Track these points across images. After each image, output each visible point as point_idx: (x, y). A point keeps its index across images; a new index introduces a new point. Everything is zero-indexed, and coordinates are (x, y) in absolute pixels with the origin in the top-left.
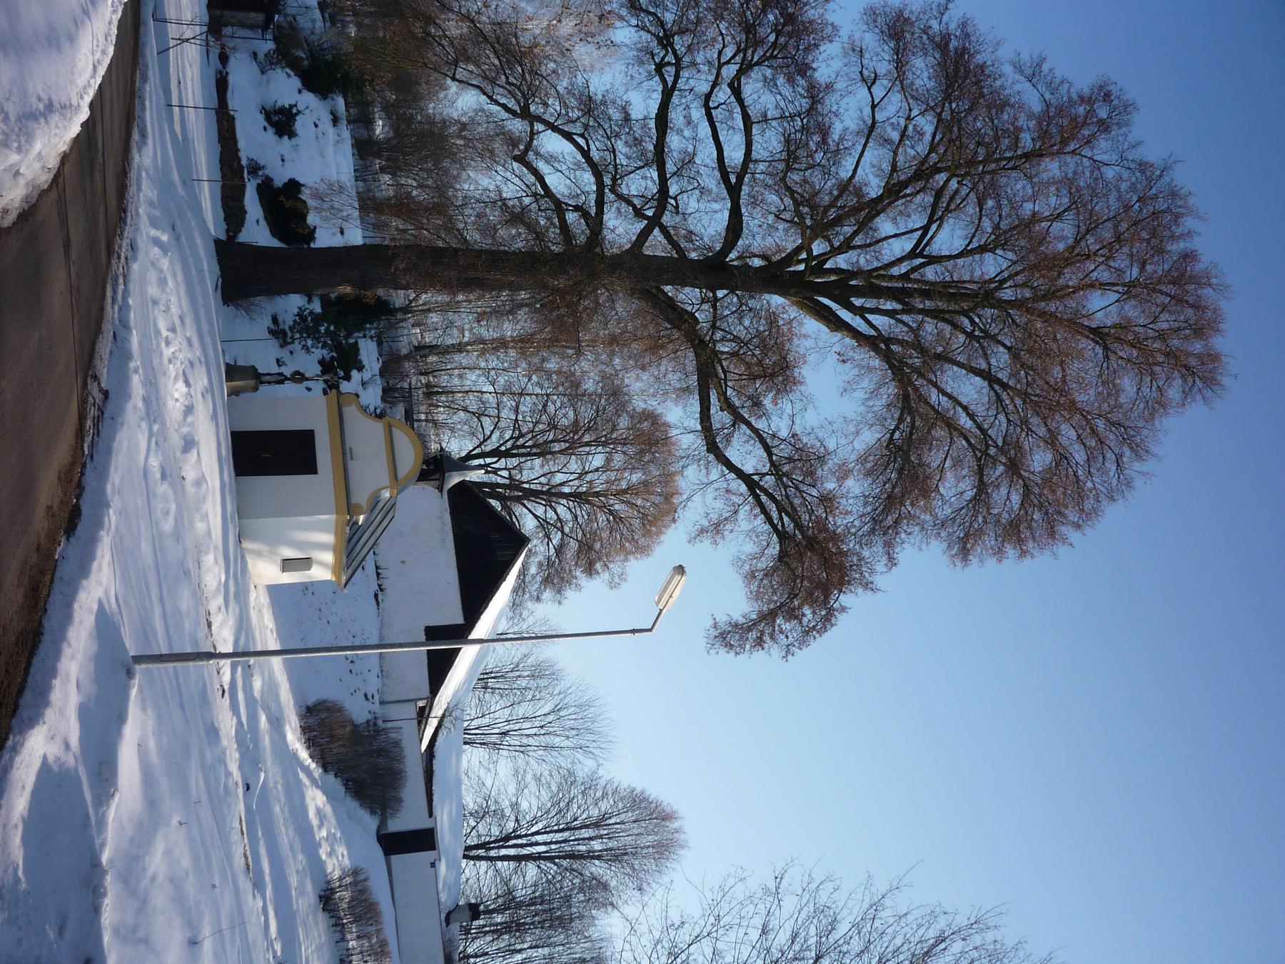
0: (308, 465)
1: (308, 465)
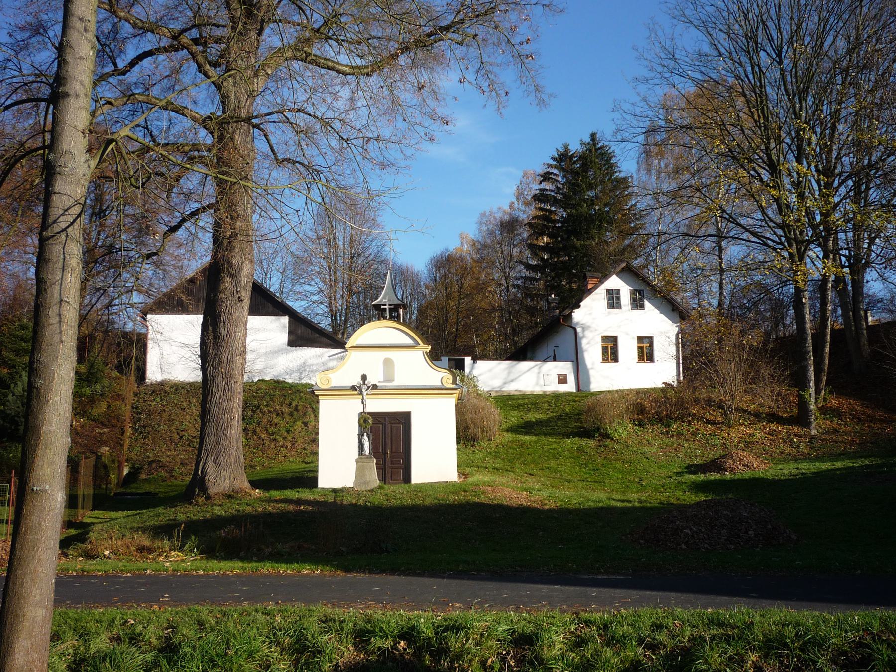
0: (404, 419)
1: (404, 419)
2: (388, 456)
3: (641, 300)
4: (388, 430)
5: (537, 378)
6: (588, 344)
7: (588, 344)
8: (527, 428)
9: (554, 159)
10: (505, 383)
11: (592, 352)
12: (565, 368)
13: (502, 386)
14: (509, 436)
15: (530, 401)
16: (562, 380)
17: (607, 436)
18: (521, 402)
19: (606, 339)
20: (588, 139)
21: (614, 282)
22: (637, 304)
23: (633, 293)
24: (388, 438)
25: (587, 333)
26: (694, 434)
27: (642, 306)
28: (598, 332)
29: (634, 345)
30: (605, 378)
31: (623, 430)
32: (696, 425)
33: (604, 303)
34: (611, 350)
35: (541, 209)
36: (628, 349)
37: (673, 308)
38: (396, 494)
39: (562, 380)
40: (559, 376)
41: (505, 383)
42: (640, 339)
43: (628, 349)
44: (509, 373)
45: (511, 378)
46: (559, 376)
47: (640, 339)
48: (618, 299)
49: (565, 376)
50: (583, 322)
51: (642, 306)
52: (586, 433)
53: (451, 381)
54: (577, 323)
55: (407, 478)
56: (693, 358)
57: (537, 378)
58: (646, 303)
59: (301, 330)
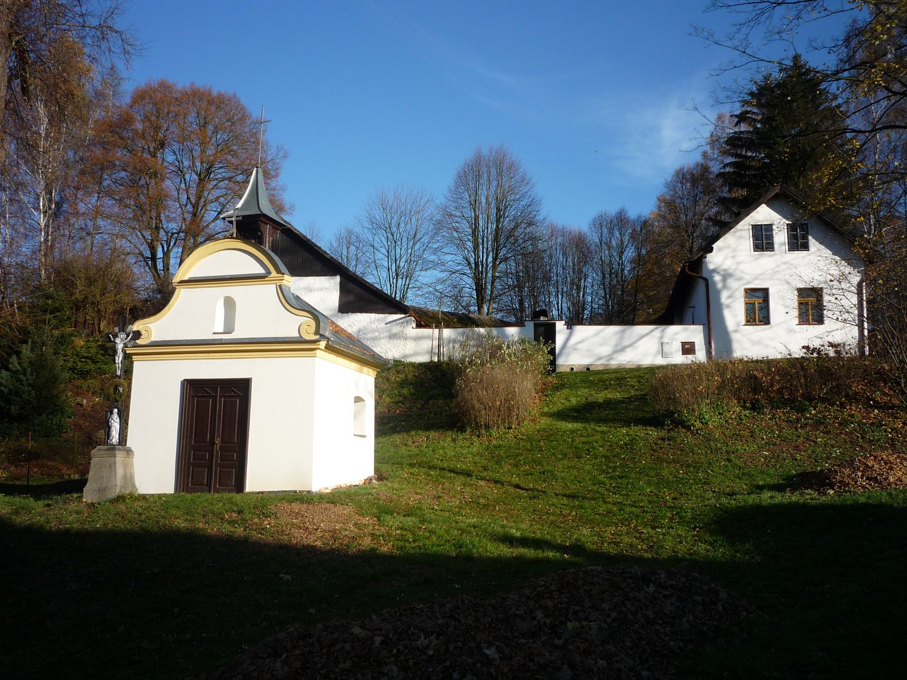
0: (238, 392)
1: (238, 392)
2: (217, 447)
3: (805, 237)
4: (220, 407)
5: (652, 347)
6: (730, 297)
7: (730, 297)
8: (583, 412)
9: (751, 94)
10: (615, 352)
11: (734, 313)
12: (694, 333)
13: (610, 357)
14: (545, 422)
15: (613, 376)
16: (688, 348)
17: (681, 423)
18: (605, 377)
19: (750, 292)
20: (789, 63)
21: (763, 214)
22: (798, 243)
23: (791, 228)
24: (216, 418)
25: (731, 282)
26: (844, 423)
27: (805, 247)
28: (743, 282)
29: (793, 300)
30: (752, 344)
31: (713, 417)
32: (856, 410)
33: (749, 243)
34: (758, 308)
35: (737, 155)
36: (784, 306)
37: (843, 238)
38: (212, 516)
39: (688, 348)
40: (683, 344)
41: (615, 352)
42: (802, 292)
43: (784, 306)
44: (621, 339)
45: (626, 342)
46: (683, 344)
47: (802, 292)
48: (770, 237)
49: (692, 344)
50: (725, 267)
51: (805, 247)
52: (655, 421)
53: (313, 329)
54: (714, 271)
55: (240, 485)
56: (877, 311)
57: (652, 347)
58: (812, 241)
59: (351, 286)
